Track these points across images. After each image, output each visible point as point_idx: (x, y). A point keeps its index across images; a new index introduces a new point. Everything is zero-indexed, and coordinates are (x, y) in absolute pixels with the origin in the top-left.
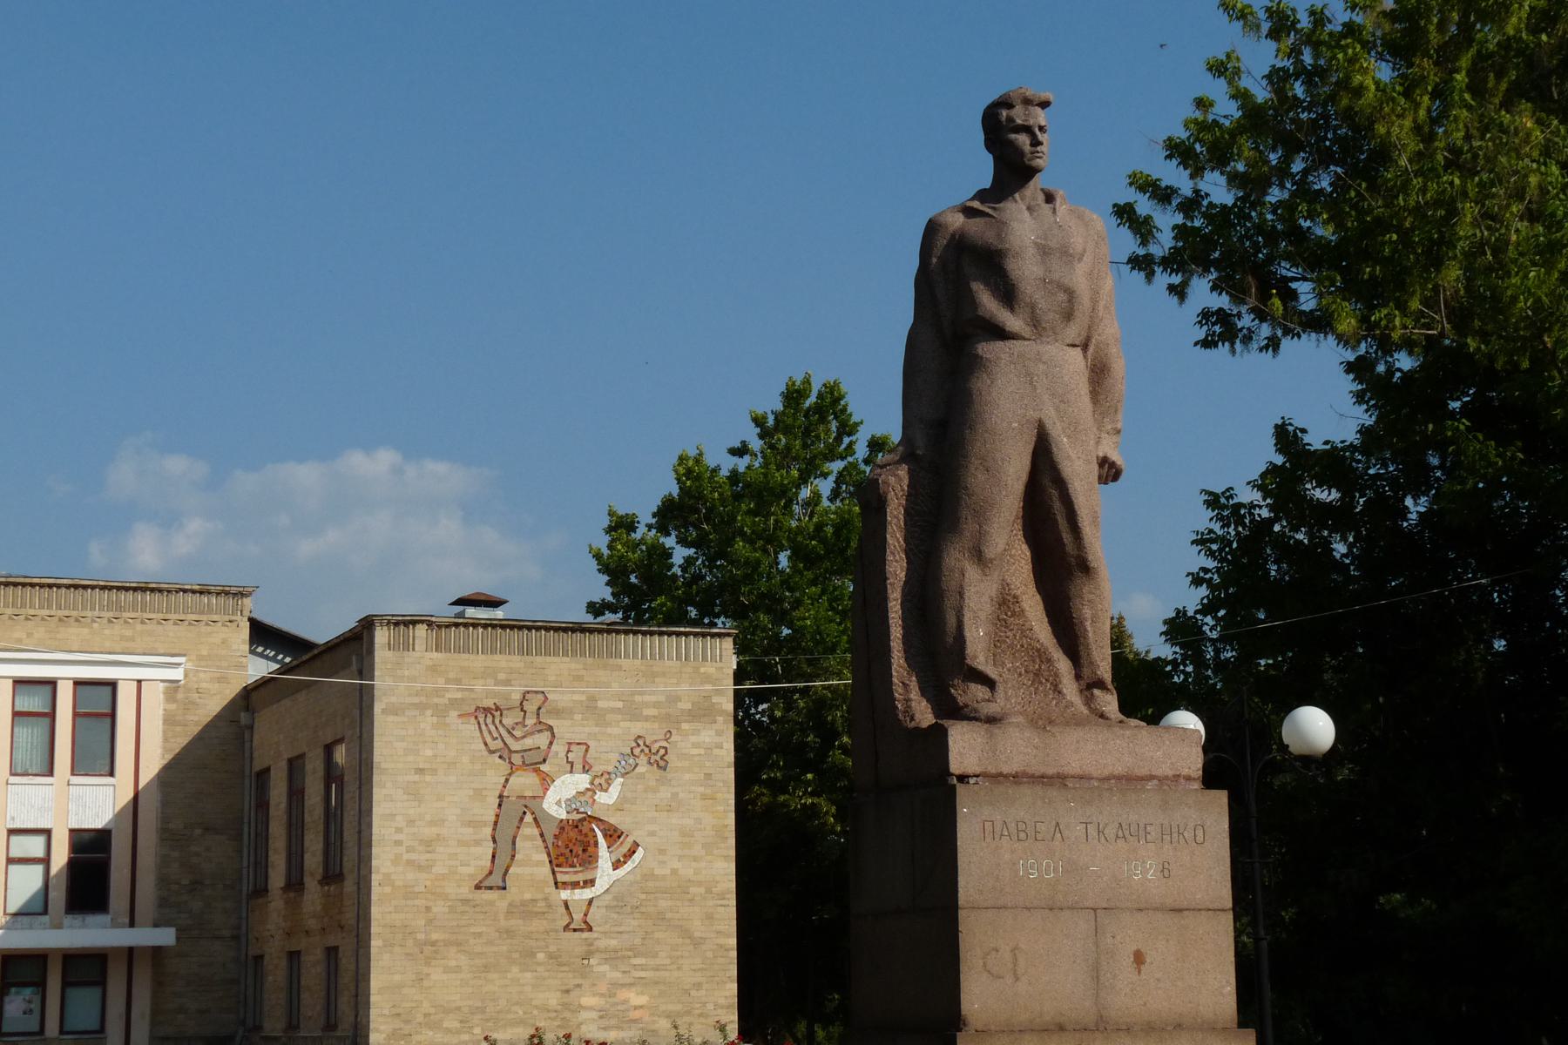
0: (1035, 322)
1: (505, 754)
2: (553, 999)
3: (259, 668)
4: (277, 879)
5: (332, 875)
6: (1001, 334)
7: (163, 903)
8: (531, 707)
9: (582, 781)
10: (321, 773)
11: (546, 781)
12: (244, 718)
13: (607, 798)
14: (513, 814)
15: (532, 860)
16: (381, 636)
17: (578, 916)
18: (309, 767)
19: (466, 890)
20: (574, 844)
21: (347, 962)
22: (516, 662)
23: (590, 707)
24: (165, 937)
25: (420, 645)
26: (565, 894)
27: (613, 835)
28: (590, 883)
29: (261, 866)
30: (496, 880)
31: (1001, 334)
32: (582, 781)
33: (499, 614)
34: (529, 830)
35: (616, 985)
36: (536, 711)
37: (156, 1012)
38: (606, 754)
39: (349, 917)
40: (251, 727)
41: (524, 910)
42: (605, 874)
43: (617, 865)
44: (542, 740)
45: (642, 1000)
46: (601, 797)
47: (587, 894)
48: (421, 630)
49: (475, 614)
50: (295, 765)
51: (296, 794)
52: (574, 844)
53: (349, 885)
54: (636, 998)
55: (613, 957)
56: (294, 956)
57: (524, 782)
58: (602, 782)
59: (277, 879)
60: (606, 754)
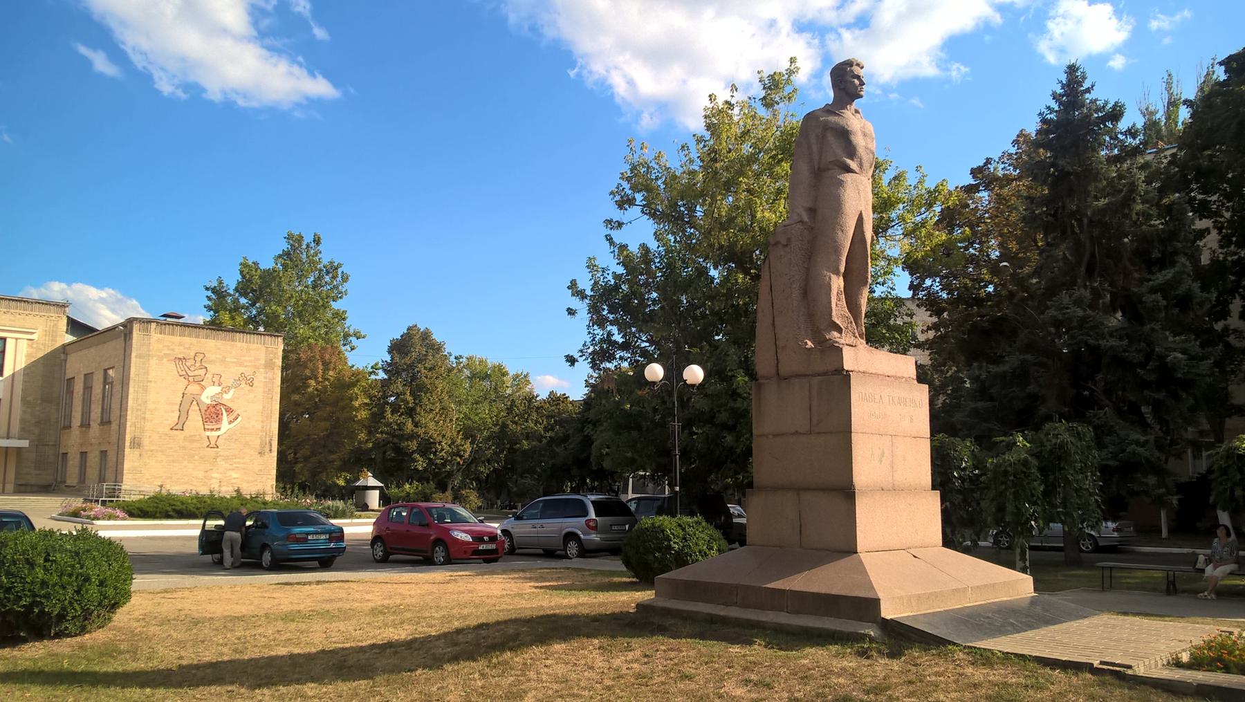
0: (861, 166)
1: (186, 377)
2: (201, 474)
3: (70, 338)
4: (76, 421)
5: (105, 422)
6: (849, 170)
7: (22, 429)
8: (198, 359)
9: (218, 389)
10: (102, 380)
11: (203, 388)
12: (62, 356)
13: (227, 396)
14: (186, 403)
15: (195, 420)
16: (136, 327)
17: (213, 442)
18: (95, 378)
19: (167, 430)
20: (213, 414)
21: (111, 456)
22: (194, 340)
23: (223, 361)
24: (25, 444)
25: (153, 333)
26: (208, 433)
27: (229, 411)
28: (219, 429)
29: (69, 417)
30: (179, 426)
31: (849, 170)
32: (218, 389)
33: (181, 321)
34: (195, 407)
35: (227, 469)
36: (200, 359)
37: (17, 473)
38: (228, 379)
39: (114, 438)
40: (66, 361)
41: (191, 439)
42: (225, 426)
43: (230, 422)
44: (202, 372)
45: (237, 475)
46: (225, 396)
47: (217, 433)
48: (154, 325)
49: (171, 321)
50: (88, 377)
51: (88, 388)
52: (213, 414)
53: (114, 426)
54: (234, 475)
55: (226, 459)
56: (84, 454)
57: (194, 388)
58: (226, 390)
59: (76, 421)
60: (228, 379)
